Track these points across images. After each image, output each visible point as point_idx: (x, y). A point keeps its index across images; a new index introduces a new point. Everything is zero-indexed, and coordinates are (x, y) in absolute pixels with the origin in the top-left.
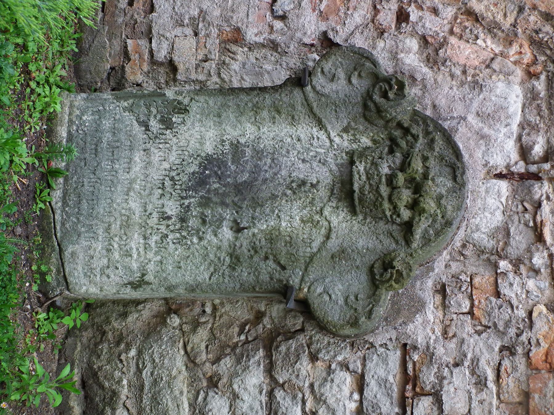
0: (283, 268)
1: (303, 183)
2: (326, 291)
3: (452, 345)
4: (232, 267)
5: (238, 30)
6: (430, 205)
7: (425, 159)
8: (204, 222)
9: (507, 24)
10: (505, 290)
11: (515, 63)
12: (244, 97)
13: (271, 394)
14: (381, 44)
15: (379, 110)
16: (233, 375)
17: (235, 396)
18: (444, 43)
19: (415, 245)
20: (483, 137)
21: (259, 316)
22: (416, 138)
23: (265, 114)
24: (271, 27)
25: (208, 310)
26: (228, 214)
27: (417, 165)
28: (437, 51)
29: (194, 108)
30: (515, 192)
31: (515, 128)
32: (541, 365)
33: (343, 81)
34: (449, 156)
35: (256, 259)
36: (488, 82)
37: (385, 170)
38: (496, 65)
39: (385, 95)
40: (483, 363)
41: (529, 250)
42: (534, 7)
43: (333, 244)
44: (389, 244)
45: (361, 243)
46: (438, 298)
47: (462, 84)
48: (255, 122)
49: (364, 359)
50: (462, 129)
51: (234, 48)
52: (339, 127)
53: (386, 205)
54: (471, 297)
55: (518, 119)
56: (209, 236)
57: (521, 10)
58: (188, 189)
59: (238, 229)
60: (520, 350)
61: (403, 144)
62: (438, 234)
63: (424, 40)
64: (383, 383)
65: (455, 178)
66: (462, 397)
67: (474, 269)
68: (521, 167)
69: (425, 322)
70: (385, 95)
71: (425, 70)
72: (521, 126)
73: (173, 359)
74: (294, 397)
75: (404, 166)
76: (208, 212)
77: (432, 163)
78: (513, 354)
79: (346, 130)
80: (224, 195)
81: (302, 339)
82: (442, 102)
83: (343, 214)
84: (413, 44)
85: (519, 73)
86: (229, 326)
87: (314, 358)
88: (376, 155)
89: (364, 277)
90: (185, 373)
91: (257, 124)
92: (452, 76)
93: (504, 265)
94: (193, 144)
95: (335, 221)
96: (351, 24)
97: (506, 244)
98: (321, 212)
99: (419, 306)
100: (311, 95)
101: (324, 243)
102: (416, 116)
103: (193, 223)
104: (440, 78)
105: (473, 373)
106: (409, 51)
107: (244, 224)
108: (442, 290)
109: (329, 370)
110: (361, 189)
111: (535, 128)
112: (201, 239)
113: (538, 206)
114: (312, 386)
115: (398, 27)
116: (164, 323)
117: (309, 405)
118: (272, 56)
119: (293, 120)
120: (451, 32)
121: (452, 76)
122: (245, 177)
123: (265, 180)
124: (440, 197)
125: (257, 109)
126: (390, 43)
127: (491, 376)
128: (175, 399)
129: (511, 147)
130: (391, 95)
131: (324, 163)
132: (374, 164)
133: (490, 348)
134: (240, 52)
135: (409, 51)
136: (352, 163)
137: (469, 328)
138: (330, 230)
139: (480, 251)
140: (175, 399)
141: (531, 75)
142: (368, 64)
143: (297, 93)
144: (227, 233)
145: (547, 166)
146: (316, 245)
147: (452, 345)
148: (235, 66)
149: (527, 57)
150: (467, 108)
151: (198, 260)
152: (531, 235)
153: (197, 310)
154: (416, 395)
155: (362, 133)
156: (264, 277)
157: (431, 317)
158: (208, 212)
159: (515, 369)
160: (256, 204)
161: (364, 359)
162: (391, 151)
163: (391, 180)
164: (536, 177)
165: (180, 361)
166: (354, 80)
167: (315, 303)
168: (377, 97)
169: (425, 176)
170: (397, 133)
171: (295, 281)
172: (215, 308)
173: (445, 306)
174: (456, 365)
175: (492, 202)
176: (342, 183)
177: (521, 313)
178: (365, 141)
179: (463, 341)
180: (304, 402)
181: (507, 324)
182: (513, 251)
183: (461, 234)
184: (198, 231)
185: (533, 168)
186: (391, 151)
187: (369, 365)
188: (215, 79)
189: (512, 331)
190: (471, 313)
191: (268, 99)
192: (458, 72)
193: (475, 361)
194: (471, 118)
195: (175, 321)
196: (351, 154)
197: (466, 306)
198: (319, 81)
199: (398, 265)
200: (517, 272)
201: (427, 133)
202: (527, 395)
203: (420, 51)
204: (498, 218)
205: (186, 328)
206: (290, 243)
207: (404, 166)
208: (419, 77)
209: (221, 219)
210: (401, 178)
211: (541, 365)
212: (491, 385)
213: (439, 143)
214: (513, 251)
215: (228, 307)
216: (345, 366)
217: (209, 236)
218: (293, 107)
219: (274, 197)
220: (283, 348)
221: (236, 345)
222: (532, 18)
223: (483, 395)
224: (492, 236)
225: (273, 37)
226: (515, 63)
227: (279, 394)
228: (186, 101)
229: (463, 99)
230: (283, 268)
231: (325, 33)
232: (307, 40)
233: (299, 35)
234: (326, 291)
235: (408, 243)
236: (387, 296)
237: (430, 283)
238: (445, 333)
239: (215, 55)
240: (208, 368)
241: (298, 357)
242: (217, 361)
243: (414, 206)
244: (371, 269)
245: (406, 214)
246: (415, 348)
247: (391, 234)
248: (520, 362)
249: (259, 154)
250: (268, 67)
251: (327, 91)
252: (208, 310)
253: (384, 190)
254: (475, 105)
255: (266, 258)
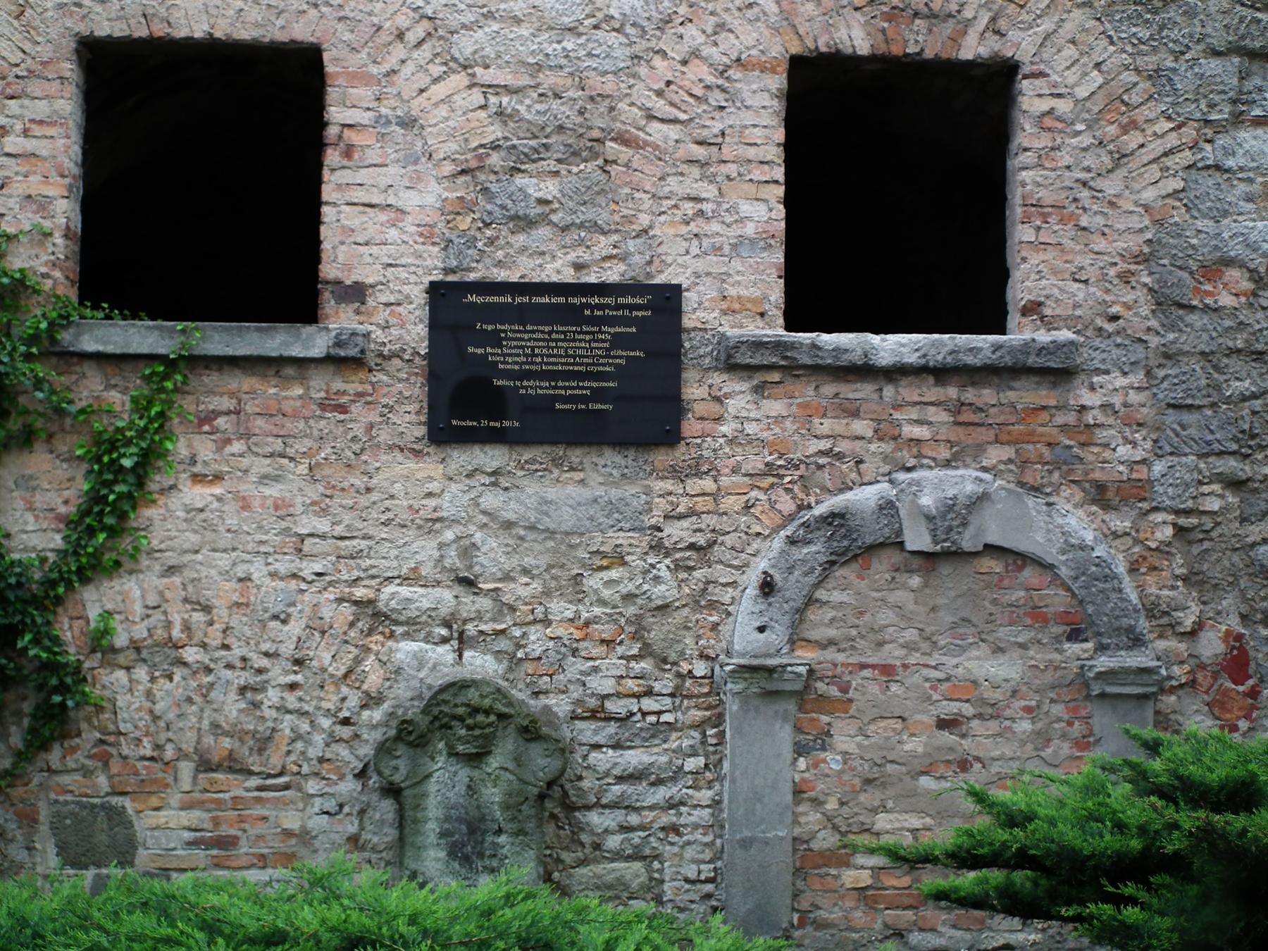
0: (527, 799)
1: (469, 787)
2: (542, 770)
3: (571, 687)
4: (526, 834)
5: (349, 839)
6: (487, 702)
7: (456, 706)
8: (495, 856)
9: (355, 651)
10: (537, 654)
11: (383, 646)
12: (407, 831)
13: (604, 807)
14: (365, 736)
15: (422, 736)
16: (593, 833)
17: (606, 831)
18: (367, 693)
19: (513, 712)
20: (434, 667)
21: (553, 816)
22: (441, 712)
23: (419, 815)
24: (348, 814)
25: (548, 852)
26: (489, 839)
27: (461, 711)
28: (372, 698)
29: (413, 866)
30: (472, 647)
31: (428, 647)
32: (584, 632)
33: (399, 761)
34: (451, 691)
35: (520, 818)
36: (396, 663)
37: (463, 732)
38: (385, 659)
39: (410, 733)
40: (583, 668)
41: (511, 639)
42: (345, 633)
43: (510, 766)
44: (512, 727)
45: (510, 747)
46: (541, 696)
47: (396, 681)
48: (426, 822)
49: (580, 745)
50: (429, 681)
51: (361, 841)
52: (430, 763)
53: (487, 731)
54: (541, 676)
55: (422, 644)
56: (505, 851)
57: (346, 642)
58: (471, 868)
59: (499, 832)
60: (575, 645)
61: (446, 720)
62: (505, 697)
63: (364, 707)
64: (596, 732)
65: (469, 687)
66: (604, 681)
67: (523, 673)
68: (455, 643)
69: (557, 705)
70: (410, 733)
71: (386, 705)
72: (427, 642)
73: (582, 876)
74: (606, 791)
75: (461, 719)
76: (488, 853)
77: (458, 701)
78: (577, 649)
79: (433, 759)
80: (476, 842)
81: (568, 786)
82: (409, 694)
83: (491, 759)
84: (366, 714)
85: (390, 643)
86: (559, 837)
87: (580, 778)
88: (452, 738)
89: (533, 745)
90: (591, 867)
91: (426, 820)
92: (390, 687)
93: (520, 655)
94: (439, 866)
95: (495, 765)
96: (352, 758)
97: (506, 652)
98: (489, 774)
99: (547, 708)
100: (407, 783)
101: (510, 772)
102: (425, 711)
103: (495, 863)
104: (391, 696)
105: (589, 674)
106: (371, 717)
107: (496, 827)
108: (536, 694)
109: (588, 767)
110: (475, 747)
111: (429, 634)
112: (506, 857)
113: (481, 632)
114: (598, 779)
115: (353, 724)
116: (558, 883)
117: (611, 781)
118: (370, 812)
119: (425, 795)
120: (358, 688)
121: (390, 687)
122: (463, 827)
123: (467, 813)
124: (482, 696)
125: (415, 821)
126: (364, 730)
127: (591, 663)
128: (609, 873)
129: (441, 649)
130: (411, 729)
131: (455, 773)
132: (459, 739)
133: (574, 663)
134: (365, 836)
135: (371, 717)
136: (457, 754)
137: (561, 677)
138: (502, 768)
139: (510, 669)
140: (609, 873)
141: (392, 635)
142: (388, 744)
143: (406, 793)
144: (502, 839)
145: (455, 626)
146: (511, 777)
147: (571, 687)
148: (375, 840)
149: (380, 638)
150: (414, 677)
151: (520, 858)
152: (501, 637)
153: (548, 860)
154: (603, 711)
155: (435, 747)
156: (533, 812)
157: (554, 701)
158: (488, 853)
159: (586, 648)
160: (482, 819)
161: (580, 745)
162: (450, 728)
163: (470, 728)
164: (461, 633)
165: (583, 871)
166: (398, 753)
167: (550, 777)
168: (411, 739)
169: (468, 705)
170: (437, 724)
171: (536, 791)
172: (547, 848)
173: (546, 692)
174: (584, 685)
175: (478, 662)
176: (469, 760)
177: (551, 644)
178: (441, 745)
179: (569, 681)
180: (609, 784)
181: (558, 653)
182: (511, 649)
183: (500, 681)
184: (501, 859)
185: (456, 635)
186: (450, 728)
187: (584, 741)
188: (384, 854)
189: (563, 650)
190: (551, 676)
191: (409, 813)
192: (388, 683)
193: (582, 673)
194: (421, 675)
195: (556, 875)
196: (450, 755)
197: (547, 679)
198: (397, 778)
199: (525, 723)
200: (524, 646)
201: (438, 704)
202: (603, 641)
203: (372, 709)
204: (489, 657)
205: (561, 867)
206: (510, 795)
207: (461, 719)
208: (391, 710)
209: (493, 843)
210: (469, 721)
211: (584, 632)
212: (597, 663)
213: (445, 696)
214: (511, 649)
215: (547, 838)
216: (585, 757)
217: (505, 851)
218: (415, 796)
219: (478, 807)
220: (574, 799)
221: (573, 832)
222: (352, 634)
223: (603, 668)
224: (500, 661)
225: (355, 813)
226: (383, 646)
227: (604, 801)
228: (408, 872)
229: (407, 680)
230: (527, 799)
231: (355, 776)
232: (359, 788)
233: (355, 794)
234: (542, 770)
235: (511, 716)
236: (545, 730)
237: (532, 702)
238: (563, 692)
239: (366, 854)
240: (588, 850)
241: (580, 789)
242: (582, 845)
243: (487, 712)
244: (528, 740)
245: (492, 718)
246: (573, 711)
247: (505, 728)
248: (583, 645)
249: (447, 819)
250: (377, 816)
251: (405, 772)
252: (548, 852)
253: (477, 732)
254: (412, 672)
255: (520, 811)
